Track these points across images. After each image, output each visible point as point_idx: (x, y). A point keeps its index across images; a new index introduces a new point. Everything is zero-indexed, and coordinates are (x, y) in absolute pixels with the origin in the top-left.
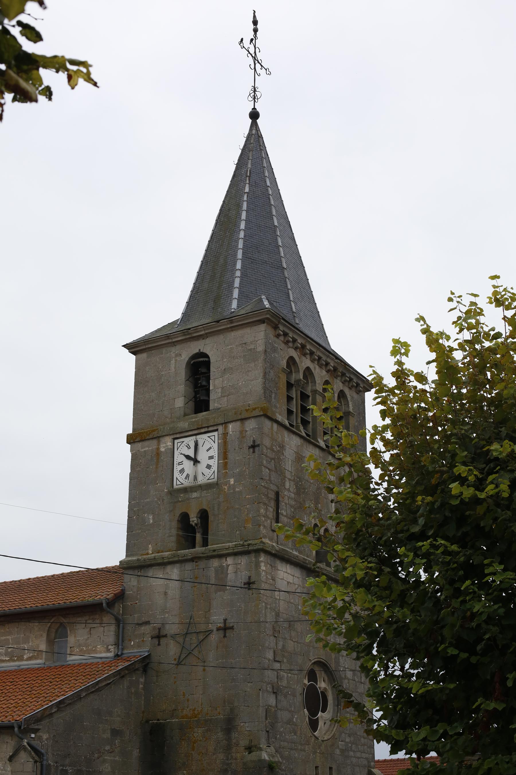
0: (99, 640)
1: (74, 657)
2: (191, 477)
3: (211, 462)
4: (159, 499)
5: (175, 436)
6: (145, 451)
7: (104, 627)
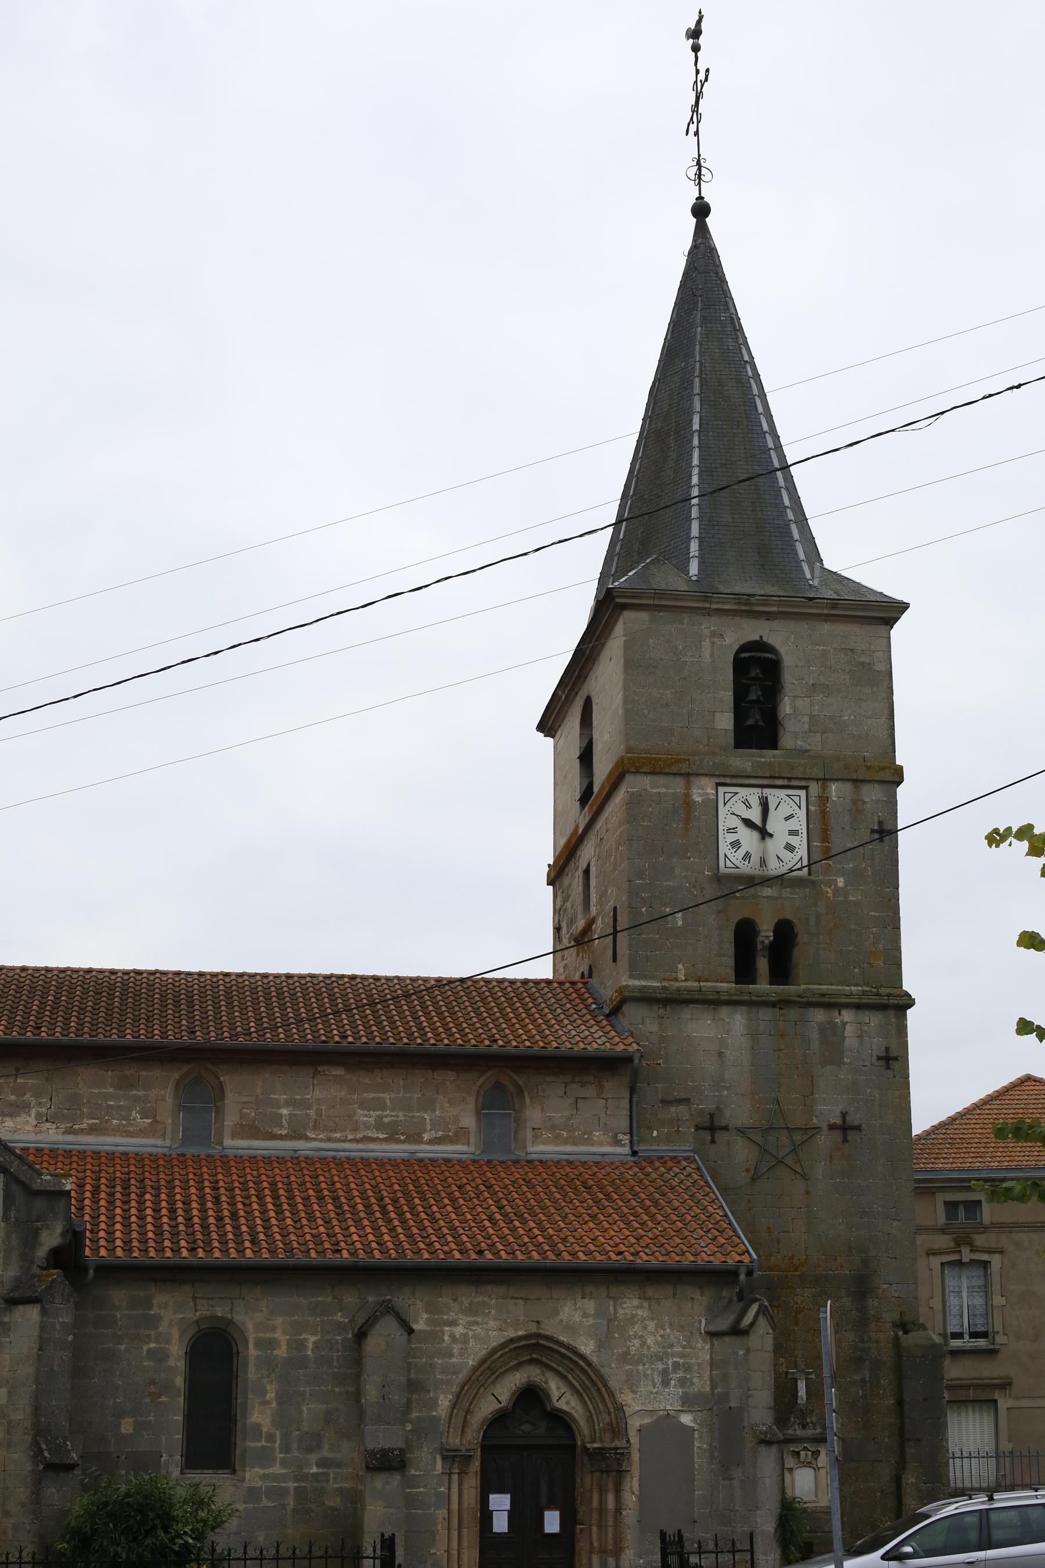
0: (596, 1121)
1: (541, 1148)
2: (755, 859)
3: (794, 841)
4: (695, 887)
5: (722, 780)
6: (659, 793)
7: (606, 1100)
